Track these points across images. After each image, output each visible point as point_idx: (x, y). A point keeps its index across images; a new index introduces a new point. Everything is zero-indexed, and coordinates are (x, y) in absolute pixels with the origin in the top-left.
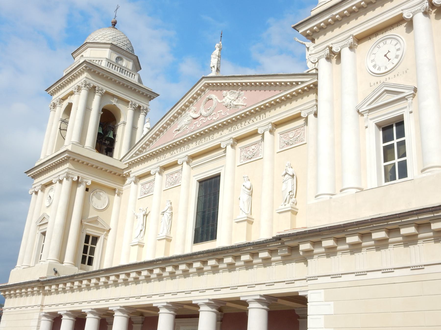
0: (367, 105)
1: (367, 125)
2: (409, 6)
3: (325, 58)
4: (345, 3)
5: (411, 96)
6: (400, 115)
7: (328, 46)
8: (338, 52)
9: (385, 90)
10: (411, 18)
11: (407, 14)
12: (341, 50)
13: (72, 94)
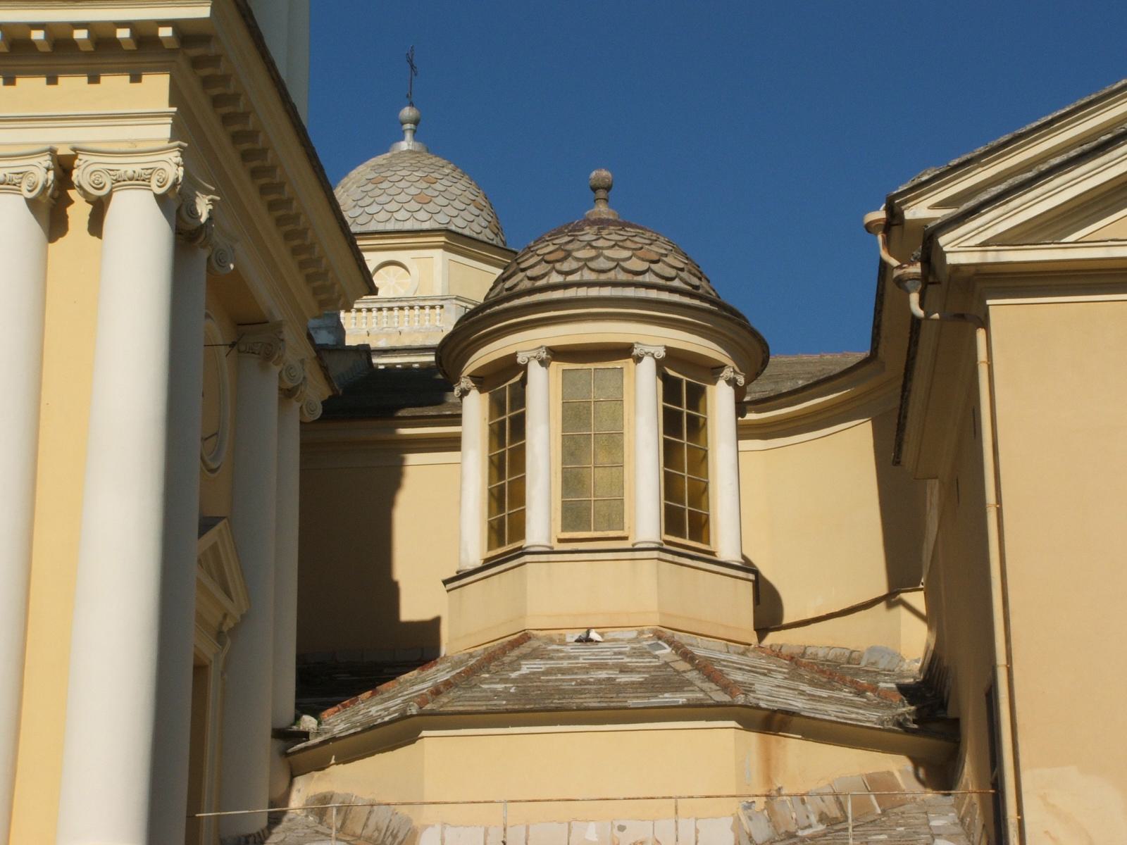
11: (93, 177)
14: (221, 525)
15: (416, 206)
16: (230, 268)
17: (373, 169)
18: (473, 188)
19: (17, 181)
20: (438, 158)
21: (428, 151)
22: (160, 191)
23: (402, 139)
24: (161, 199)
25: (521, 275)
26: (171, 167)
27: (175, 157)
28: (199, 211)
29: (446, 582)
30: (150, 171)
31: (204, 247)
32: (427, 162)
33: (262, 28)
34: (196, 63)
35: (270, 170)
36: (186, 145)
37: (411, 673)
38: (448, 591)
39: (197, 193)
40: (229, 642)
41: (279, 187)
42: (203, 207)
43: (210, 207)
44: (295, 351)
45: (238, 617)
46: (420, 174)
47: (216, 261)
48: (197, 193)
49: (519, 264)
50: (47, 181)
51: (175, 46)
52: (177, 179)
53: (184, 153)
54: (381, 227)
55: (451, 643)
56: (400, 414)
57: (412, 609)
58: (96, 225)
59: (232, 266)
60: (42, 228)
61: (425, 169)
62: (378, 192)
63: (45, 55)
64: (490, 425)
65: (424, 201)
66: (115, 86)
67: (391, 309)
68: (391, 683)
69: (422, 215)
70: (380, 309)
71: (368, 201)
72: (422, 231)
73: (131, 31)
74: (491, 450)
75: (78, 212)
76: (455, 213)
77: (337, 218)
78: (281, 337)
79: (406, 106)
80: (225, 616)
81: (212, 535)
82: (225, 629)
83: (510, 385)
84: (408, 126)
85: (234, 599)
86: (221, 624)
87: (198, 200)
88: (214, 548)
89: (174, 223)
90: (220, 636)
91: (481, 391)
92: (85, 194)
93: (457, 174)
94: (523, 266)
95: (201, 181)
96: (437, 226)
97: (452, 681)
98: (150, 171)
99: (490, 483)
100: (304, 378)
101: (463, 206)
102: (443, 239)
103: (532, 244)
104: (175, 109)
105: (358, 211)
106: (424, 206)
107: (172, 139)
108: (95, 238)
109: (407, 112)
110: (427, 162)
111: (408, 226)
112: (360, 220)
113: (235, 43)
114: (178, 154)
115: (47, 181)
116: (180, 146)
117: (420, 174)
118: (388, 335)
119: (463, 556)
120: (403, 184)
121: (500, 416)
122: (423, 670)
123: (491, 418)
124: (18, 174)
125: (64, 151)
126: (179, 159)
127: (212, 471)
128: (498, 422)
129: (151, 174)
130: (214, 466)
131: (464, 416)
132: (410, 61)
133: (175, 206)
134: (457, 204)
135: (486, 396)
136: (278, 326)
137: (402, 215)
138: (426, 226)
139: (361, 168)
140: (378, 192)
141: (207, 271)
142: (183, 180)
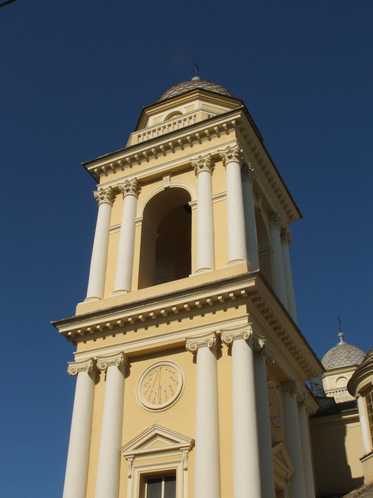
0: (132, 449)
1: (187, 467)
2: (230, 327)
3: (208, 348)
4: (96, 317)
5: (133, 457)
6: (147, 473)
7: (92, 359)
8: (227, 343)
9: (156, 433)
10: (195, 351)
11: (227, 338)
12: (197, 349)
13: (188, 168)
14: (281, 444)
15: (346, 360)
16: (273, 362)
17: (332, 351)
18: (362, 352)
19: (206, 343)
20: (351, 345)
21: (347, 344)
22: (246, 338)
23: (340, 342)
24: (247, 341)
25: (369, 358)
26: (249, 331)
27: (250, 327)
28: (260, 344)
29: (361, 459)
30: (243, 333)
31: (264, 356)
32: (347, 347)
33: (282, 303)
34: (254, 300)
35: (298, 353)
36: (252, 323)
37: (354, 491)
38: (362, 462)
39: (259, 339)
40: (290, 482)
41: (284, 333)
42: (261, 343)
43: (264, 343)
44: (300, 389)
45: (292, 474)
46: (346, 350)
47: (268, 361)
48: (259, 339)
49: (368, 355)
50: (214, 341)
51: (247, 296)
52: (251, 334)
53: (252, 326)
54: (337, 367)
55: (367, 482)
56: (342, 412)
57: (355, 474)
58: (230, 353)
59: (274, 362)
60: (215, 355)
61: (347, 349)
62: (334, 357)
63: (212, 306)
64: (367, 407)
65: (348, 358)
66: (232, 312)
67: (343, 391)
68: (347, 495)
69: (348, 362)
70: (340, 391)
71: (332, 360)
72: (349, 366)
73: (233, 294)
74: (368, 414)
75: (225, 349)
76: (358, 360)
77: (312, 353)
78: (295, 385)
79: (339, 333)
80: (287, 474)
81: (278, 447)
82: (288, 478)
83: (371, 393)
84: (341, 338)
85: (290, 468)
86: (286, 477)
87: (259, 341)
88: (280, 451)
89: (252, 348)
90: (286, 481)
91: (363, 396)
92: (225, 343)
93: (357, 349)
94: (370, 355)
95: (259, 335)
96: (353, 364)
97: (365, 489)
98: (243, 333)
99: (370, 425)
100: (305, 398)
101: (360, 358)
102: (355, 368)
103: (372, 348)
104: (248, 314)
105: (330, 364)
106: (349, 359)
107: (249, 322)
108: (230, 356)
109: (340, 334)
110: (347, 347)
111: (345, 366)
112: (330, 366)
113: (264, 293)
114: (250, 326)
115: (214, 341)
116: (250, 324)
117: (346, 350)
118: (343, 398)
119: (365, 450)
120: (341, 354)
121: (370, 403)
122: (357, 490)
123: (367, 404)
124: (206, 341)
125: (218, 332)
126: (251, 328)
127: (278, 428)
128: (370, 405)
129: (243, 334)
130: (278, 426)
131: (358, 403)
132: (339, 320)
133: (252, 343)
134: (358, 357)
135: (364, 398)
136: (294, 382)
137: (342, 363)
138: (350, 365)
139: (329, 352)
140: (334, 357)
141: (266, 363)
142: (253, 334)
